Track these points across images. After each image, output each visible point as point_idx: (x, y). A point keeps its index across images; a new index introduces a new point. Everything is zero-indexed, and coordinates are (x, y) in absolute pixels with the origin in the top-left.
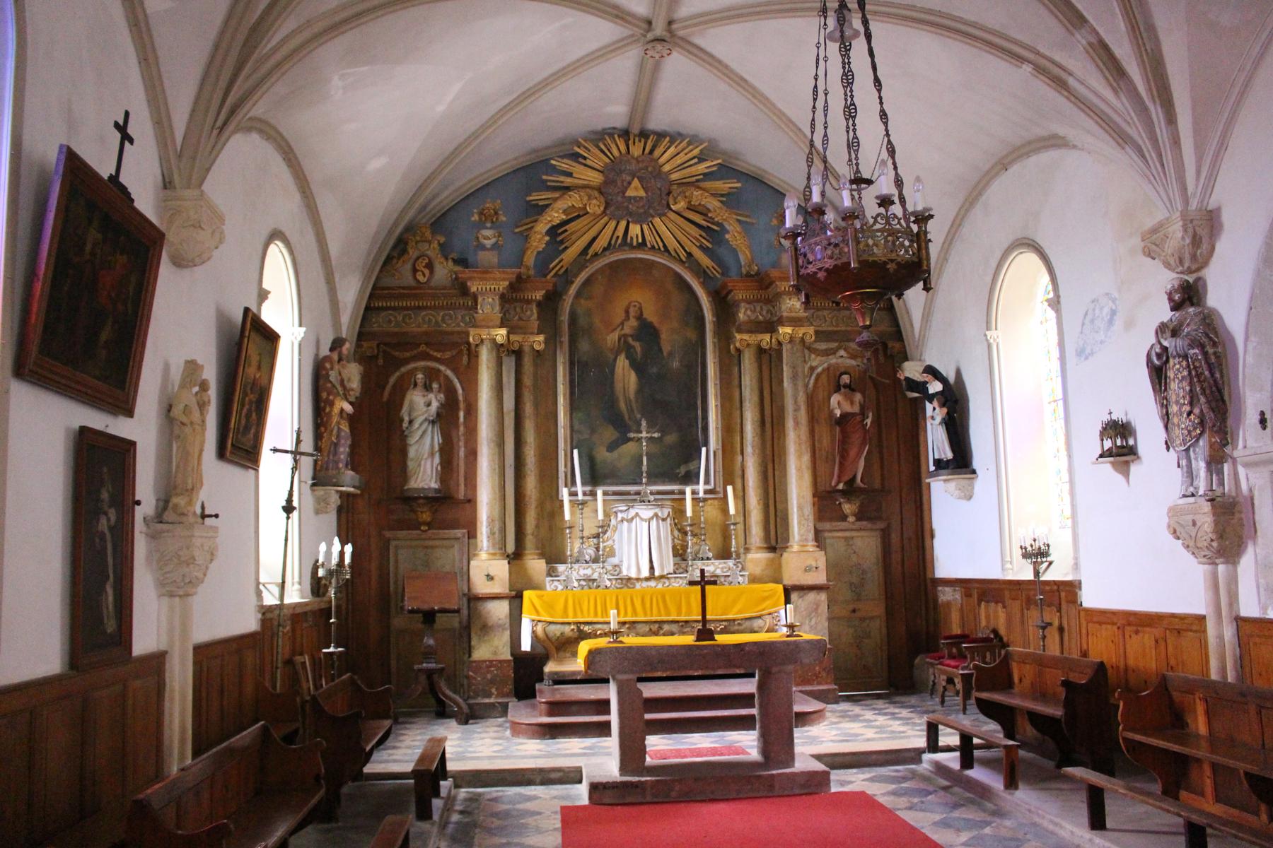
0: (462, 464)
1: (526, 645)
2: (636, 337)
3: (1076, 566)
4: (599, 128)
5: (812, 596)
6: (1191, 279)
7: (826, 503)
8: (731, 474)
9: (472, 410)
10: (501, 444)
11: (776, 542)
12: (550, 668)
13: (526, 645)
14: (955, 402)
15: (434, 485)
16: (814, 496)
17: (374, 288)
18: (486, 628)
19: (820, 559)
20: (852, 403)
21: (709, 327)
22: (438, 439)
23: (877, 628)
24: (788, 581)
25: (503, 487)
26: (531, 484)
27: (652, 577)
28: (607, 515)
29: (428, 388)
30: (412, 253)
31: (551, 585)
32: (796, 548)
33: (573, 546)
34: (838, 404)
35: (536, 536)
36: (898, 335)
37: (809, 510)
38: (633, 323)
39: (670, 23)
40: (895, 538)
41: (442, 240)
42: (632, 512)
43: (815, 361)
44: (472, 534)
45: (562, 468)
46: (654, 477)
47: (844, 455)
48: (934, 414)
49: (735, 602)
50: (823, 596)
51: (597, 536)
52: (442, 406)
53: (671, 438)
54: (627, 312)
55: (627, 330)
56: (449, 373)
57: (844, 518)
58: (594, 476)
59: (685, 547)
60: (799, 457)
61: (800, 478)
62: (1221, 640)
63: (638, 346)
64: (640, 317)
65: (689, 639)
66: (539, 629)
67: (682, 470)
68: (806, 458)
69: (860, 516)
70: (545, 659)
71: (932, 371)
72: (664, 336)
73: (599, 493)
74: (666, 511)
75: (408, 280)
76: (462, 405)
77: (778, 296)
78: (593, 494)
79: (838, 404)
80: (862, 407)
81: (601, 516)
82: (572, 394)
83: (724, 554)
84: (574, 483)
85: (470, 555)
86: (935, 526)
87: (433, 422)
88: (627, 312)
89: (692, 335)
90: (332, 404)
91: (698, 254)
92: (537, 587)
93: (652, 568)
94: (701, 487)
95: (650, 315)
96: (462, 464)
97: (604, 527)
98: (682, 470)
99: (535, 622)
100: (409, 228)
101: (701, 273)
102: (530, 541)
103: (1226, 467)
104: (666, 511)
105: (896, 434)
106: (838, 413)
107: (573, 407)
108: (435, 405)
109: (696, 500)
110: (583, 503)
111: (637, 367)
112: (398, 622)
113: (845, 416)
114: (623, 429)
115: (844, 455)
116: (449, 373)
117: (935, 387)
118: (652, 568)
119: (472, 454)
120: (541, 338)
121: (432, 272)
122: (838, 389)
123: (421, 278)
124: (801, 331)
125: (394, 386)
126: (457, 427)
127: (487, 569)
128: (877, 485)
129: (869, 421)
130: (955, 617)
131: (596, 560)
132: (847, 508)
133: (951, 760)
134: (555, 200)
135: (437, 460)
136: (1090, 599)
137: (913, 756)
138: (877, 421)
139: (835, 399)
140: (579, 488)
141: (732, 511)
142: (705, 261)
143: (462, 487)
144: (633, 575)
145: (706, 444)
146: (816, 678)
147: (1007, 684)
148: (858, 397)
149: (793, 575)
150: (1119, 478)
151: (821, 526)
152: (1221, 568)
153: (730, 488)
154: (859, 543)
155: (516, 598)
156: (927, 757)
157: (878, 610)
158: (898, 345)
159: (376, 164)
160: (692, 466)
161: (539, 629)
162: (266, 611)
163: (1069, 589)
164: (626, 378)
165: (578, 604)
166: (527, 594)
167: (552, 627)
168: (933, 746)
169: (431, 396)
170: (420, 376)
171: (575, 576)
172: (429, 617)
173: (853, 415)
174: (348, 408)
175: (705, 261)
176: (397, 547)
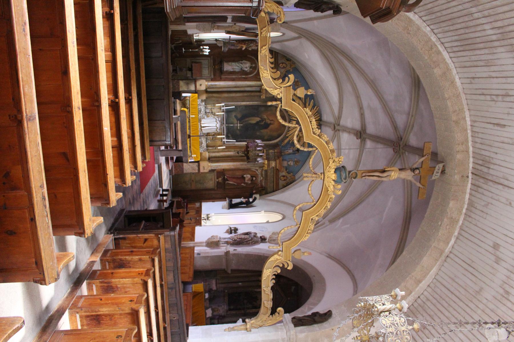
0: (230, 77)
1: (184, 95)
2: (265, 123)
3: (205, 226)
4: (322, 113)
5: (197, 168)
6: (267, 240)
7: (221, 173)
8: (228, 148)
9: (245, 79)
10: (235, 87)
11: (211, 159)
12: (178, 101)
13: (184, 95)
14: (248, 205)
15: (225, 69)
16: (223, 169)
17: (278, 53)
18: (188, 84)
19: (206, 171)
20: (248, 180)
21: (268, 142)
22: (237, 70)
23: (189, 187)
24: (201, 162)
25: (223, 88)
26: (226, 95)
27: (201, 127)
28: (218, 115)
29: (251, 67)
30: (287, 63)
31: (199, 101)
32: (209, 164)
33: (209, 107)
34: (248, 177)
35: (212, 95)
36: (267, 193)
37: (219, 168)
38: (269, 122)
39: (339, 130)
40: (213, 192)
41: (291, 71)
42: (218, 122)
43: (259, 171)
44: (212, 80)
45: (230, 103)
46: (228, 128)
47: (234, 178)
48: (243, 200)
49: (195, 148)
50: (197, 171)
51: (212, 113)
52: (246, 71)
53: (238, 132)
54: (272, 120)
55: (267, 120)
56: (255, 73)
57: (218, 178)
58: (228, 112)
59: (209, 136)
60: (233, 165)
61: (227, 166)
62: (191, 244)
63: (263, 123)
64: (271, 124)
65: (188, 133)
66: (188, 98)
67: (230, 135)
68: (233, 167)
69: (218, 182)
70: (180, 100)
71: (255, 199)
72: (266, 130)
73: (223, 113)
74: (219, 131)
75: (280, 62)
76: (247, 76)
77: (275, 160)
78: (223, 112)
79: (248, 177)
80: (247, 183)
81: (217, 114)
82: (250, 106)
83: (208, 146)
84: (226, 106)
85: (207, 80)
86: (216, 203)
87: (241, 69)
88: (272, 120)
89: (266, 138)
90: (245, 44)
91: (288, 139)
92: (198, 98)
93: (204, 127)
94: (225, 140)
95: (271, 127)
96: (230, 77)
97: (214, 115)
98: (230, 135)
99: (190, 97)
100: (294, 63)
101: (283, 140)
102: (211, 95)
103: (226, 245)
104: (219, 131)
105: (239, 192)
106: (245, 176)
107: (246, 106)
108: (246, 69)
109: (222, 139)
110: (221, 109)
111: (257, 123)
112: (189, 60)
113: (244, 178)
114: (240, 120)
115: (234, 178)
116: (255, 73)
117: (251, 200)
118: (204, 127)
119: (233, 80)
120: (264, 97)
121: (282, 68)
122: (252, 177)
123: (281, 65)
124: (266, 166)
125: (251, 58)
126: (241, 75)
127: (203, 84)
128: (227, 187)
129: (243, 184)
130: (192, 206)
131: (206, 113)
132: (220, 179)
133: (161, 193)
134: (302, 101)
135: (232, 70)
136: (197, 228)
137: (161, 186)
138: (243, 187)
139: (249, 176)
140: (225, 108)
141: (219, 148)
142: (286, 141)
143: (224, 77)
144: (202, 122)
145: (237, 141)
146: (176, 170)
147: (178, 208)
148: (250, 182)
149: (203, 164)
150: (225, 231)
151: (215, 172)
152: (205, 244)
153: (224, 147)
154: (211, 182)
155: (196, 92)
156: (161, 189)
157: (193, 187)
158: (264, 193)
159: (306, 55)
160: (231, 138)
161: (188, 98)
162: (192, 35)
163: (200, 224)
164: (254, 120)
165: (194, 108)
166: (197, 95)
167: (188, 101)
168: (163, 190)
169: (248, 68)
170: (254, 65)
171: (201, 107)
172: (190, 70)
173: (245, 180)
174: (244, 49)
175: (286, 141)
176: (208, 59)
